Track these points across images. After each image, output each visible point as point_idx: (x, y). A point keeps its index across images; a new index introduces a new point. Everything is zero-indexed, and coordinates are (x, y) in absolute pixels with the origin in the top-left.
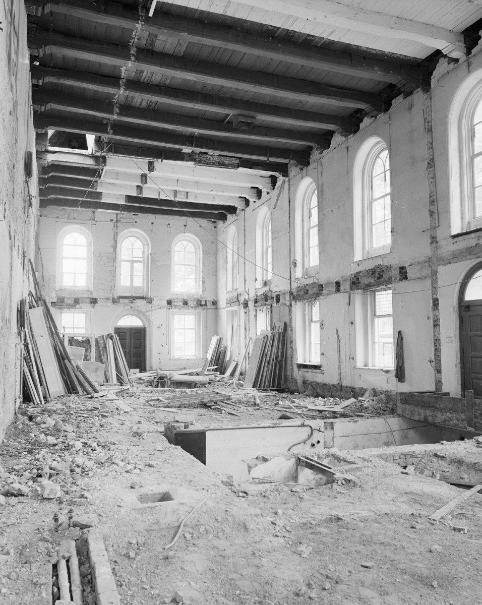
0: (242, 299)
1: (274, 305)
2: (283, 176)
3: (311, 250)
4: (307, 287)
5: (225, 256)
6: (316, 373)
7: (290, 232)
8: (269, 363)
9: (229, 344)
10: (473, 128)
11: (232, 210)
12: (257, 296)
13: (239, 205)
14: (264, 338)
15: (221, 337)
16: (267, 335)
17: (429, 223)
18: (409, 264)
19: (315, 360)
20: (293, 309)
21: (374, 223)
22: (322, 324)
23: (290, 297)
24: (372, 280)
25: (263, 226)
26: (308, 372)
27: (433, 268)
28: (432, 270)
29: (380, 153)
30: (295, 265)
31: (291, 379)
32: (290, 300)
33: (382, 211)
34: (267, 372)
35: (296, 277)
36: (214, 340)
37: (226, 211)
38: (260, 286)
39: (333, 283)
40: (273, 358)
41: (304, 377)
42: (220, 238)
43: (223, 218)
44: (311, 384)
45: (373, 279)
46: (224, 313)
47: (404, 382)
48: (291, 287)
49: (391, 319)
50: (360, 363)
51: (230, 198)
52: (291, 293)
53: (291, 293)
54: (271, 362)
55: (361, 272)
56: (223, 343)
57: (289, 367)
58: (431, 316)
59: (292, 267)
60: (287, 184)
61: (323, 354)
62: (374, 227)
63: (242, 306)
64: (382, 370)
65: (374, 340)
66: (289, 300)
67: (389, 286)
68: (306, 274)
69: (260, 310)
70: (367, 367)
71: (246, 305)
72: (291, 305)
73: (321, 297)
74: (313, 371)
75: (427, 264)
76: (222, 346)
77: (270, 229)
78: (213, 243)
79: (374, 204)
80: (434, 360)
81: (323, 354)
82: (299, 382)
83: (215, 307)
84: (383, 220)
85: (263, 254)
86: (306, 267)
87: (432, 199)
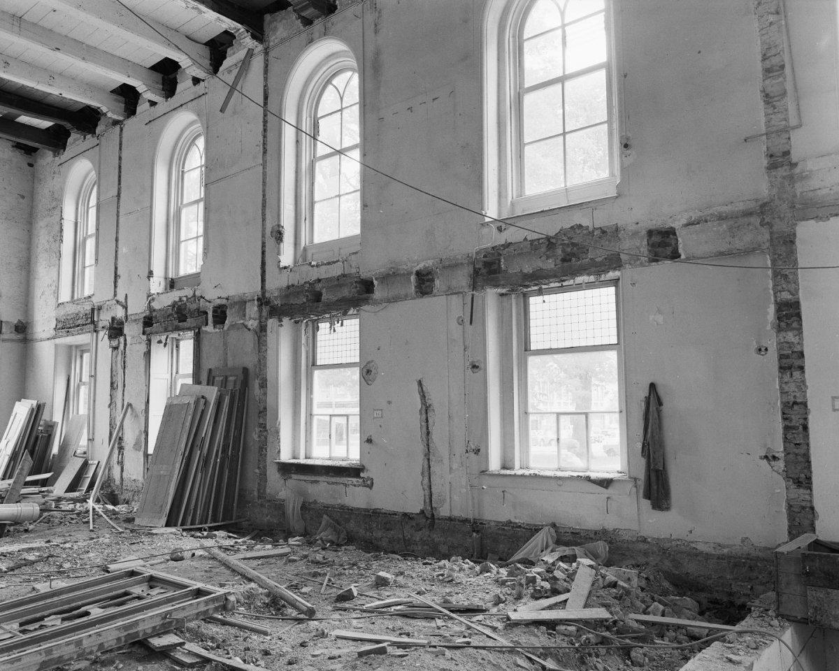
0: (105, 319)
1: (209, 328)
2: (254, 37)
3: (317, 206)
4: (318, 287)
5: (57, 228)
6: (346, 485)
7: (264, 165)
8: (206, 462)
9: (57, 418)
10: (316, 123)
11: (87, 119)
12: (151, 310)
13: (110, 108)
14: (197, 402)
15: (41, 402)
16: (203, 397)
17: (763, 120)
18: (684, 221)
19: (348, 451)
20: (270, 338)
21: (182, 238)
22: (369, 372)
23: (260, 311)
24: (550, 264)
25: (79, 193)
26: (316, 482)
27: (775, 228)
28: (771, 233)
29: (334, 75)
30: (279, 236)
31: (259, 497)
32: (260, 316)
33: (193, 223)
34: (198, 485)
35: (282, 265)
36: (22, 410)
37: (69, 122)
38: (160, 289)
39: (410, 274)
40: (217, 451)
41: (301, 493)
42: (44, 192)
43: (56, 140)
44: (327, 509)
45: (550, 261)
46: (46, 351)
47: (668, 509)
48: (263, 287)
49: (612, 356)
50: (494, 464)
51: (91, 87)
52: (263, 301)
53: (263, 301)
54: (212, 461)
55: (319, 280)
56: (45, 416)
57: (252, 471)
58: (772, 343)
59: (270, 242)
60: (257, 63)
61: (369, 441)
62: (182, 245)
63: (103, 335)
64: (588, 479)
65: (311, 409)
66: (257, 316)
67: (612, 275)
68: (303, 256)
69: (160, 342)
70: (508, 472)
71: (116, 330)
72: (263, 328)
73: (366, 307)
74: (334, 480)
75: (755, 220)
76: (42, 423)
77: (93, 201)
78: (23, 197)
79: (318, 165)
80: (781, 455)
81: (369, 441)
82: (289, 510)
83: (20, 336)
84: (195, 236)
85: (168, 219)
86: (303, 245)
87: (768, 64)
